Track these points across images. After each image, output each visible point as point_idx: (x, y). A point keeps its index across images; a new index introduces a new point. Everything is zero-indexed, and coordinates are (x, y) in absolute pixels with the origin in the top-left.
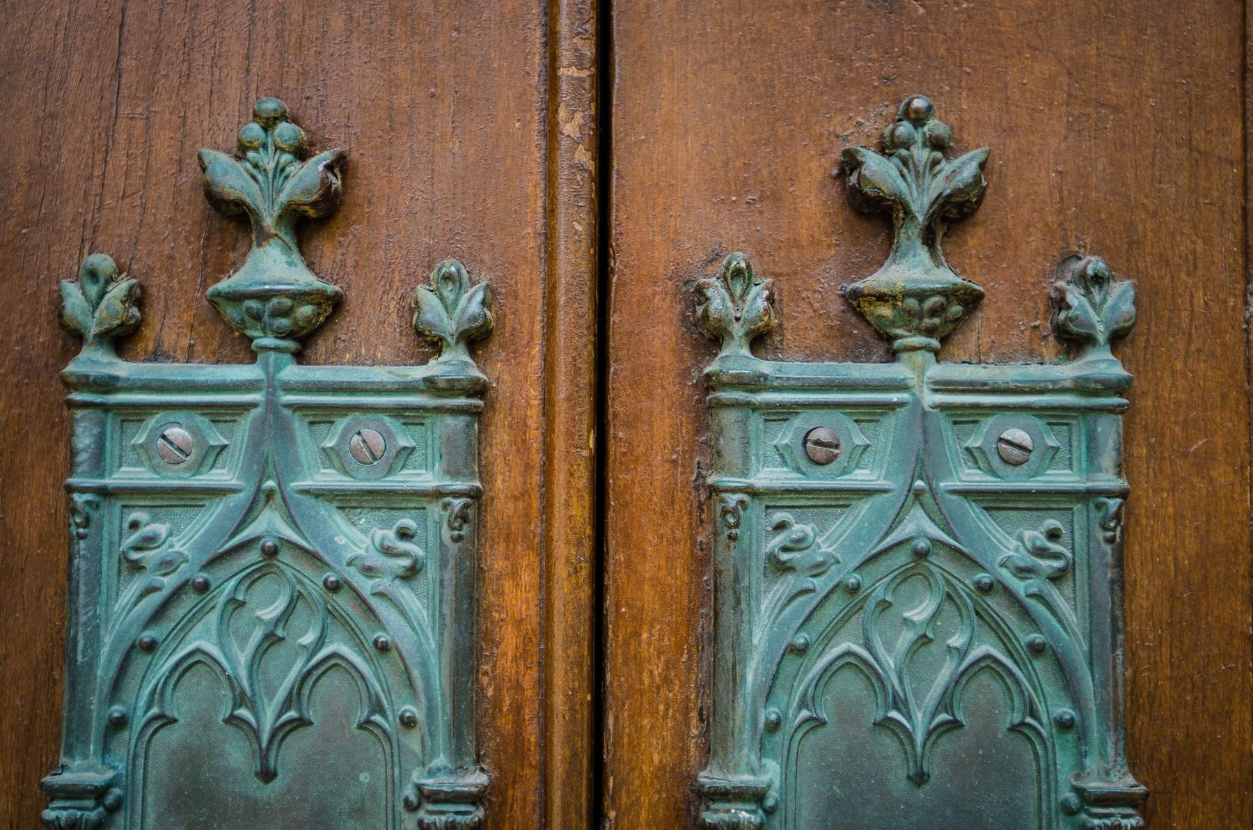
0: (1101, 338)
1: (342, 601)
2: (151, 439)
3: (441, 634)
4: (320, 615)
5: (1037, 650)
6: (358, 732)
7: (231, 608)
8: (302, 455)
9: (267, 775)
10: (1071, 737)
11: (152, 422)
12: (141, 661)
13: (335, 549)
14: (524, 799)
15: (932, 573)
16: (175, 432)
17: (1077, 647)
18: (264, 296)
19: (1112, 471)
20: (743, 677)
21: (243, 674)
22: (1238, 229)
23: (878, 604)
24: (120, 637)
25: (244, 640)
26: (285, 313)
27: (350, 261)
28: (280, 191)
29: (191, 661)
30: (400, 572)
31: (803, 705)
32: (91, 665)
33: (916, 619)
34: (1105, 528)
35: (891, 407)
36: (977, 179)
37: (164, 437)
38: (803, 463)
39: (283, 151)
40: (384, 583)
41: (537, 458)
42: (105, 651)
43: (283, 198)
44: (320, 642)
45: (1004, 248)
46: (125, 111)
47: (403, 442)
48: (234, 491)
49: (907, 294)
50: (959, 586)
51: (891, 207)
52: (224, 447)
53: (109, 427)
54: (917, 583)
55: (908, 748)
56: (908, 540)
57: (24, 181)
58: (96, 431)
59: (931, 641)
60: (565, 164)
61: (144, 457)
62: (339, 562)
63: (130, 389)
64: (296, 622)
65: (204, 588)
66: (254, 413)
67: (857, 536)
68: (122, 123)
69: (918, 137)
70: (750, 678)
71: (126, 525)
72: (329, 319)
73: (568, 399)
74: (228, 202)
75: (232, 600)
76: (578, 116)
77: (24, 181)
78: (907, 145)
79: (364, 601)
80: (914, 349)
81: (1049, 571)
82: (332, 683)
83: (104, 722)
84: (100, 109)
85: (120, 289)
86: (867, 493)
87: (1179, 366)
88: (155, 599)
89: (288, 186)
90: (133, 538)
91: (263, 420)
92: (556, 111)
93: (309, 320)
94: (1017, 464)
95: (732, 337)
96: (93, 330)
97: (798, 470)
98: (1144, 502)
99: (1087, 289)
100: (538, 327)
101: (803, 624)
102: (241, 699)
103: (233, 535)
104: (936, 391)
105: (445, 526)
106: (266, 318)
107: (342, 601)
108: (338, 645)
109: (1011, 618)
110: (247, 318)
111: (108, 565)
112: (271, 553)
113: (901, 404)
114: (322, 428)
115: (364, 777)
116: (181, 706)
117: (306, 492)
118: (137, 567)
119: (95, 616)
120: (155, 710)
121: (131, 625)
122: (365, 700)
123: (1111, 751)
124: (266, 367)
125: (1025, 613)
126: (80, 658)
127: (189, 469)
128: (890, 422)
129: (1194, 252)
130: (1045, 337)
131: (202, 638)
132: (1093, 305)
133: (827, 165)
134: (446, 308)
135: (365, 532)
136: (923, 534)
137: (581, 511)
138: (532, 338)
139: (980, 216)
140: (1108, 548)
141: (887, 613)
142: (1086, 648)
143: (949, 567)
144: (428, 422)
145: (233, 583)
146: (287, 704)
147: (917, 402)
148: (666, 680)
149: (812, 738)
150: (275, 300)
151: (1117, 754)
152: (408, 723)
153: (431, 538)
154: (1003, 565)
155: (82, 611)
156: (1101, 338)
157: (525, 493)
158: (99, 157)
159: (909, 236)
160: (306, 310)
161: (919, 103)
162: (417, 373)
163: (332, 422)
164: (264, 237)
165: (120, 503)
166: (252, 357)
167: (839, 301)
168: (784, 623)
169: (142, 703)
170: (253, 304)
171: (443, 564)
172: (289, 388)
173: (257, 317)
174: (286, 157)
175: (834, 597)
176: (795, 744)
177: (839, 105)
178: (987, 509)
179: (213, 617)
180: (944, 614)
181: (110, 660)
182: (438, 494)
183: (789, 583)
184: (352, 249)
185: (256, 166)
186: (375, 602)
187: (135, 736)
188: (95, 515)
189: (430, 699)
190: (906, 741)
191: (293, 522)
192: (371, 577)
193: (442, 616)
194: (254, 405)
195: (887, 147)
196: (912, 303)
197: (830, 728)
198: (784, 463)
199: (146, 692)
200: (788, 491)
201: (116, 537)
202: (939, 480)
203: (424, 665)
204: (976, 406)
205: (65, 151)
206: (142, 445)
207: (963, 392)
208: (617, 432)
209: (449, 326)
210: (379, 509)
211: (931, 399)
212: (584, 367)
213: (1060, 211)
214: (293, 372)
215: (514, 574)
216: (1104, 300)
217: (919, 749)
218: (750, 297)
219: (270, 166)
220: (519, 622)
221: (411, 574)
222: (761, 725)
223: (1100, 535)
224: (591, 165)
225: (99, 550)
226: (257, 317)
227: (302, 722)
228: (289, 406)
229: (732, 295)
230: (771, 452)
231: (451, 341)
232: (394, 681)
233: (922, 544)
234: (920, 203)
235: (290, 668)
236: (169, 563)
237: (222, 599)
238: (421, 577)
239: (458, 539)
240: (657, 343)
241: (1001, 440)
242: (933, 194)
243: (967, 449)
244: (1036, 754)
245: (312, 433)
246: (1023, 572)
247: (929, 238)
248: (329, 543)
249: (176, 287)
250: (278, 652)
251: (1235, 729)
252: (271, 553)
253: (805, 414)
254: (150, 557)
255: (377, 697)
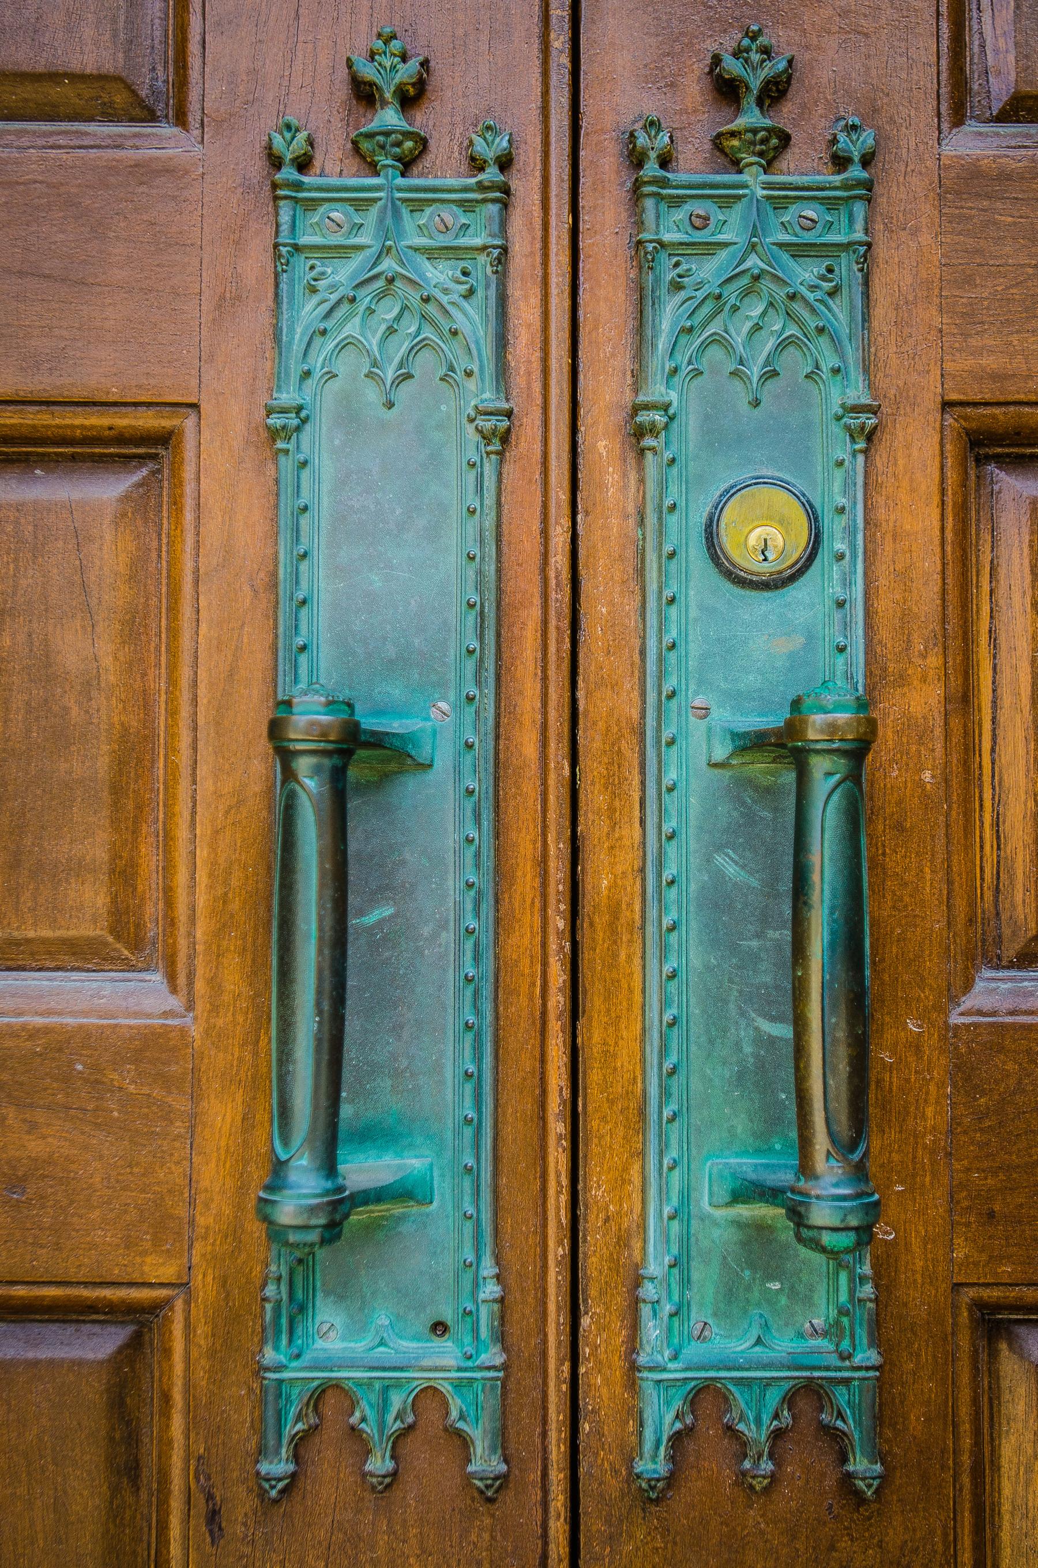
0: (856, 159)
1: (431, 309)
2: (321, 219)
3: (487, 326)
4: (418, 316)
5: (821, 330)
6: (439, 382)
7: (368, 313)
8: (407, 228)
9: (390, 405)
10: (839, 378)
11: (322, 210)
12: (318, 340)
13: (426, 279)
14: (533, 423)
15: (761, 290)
16: (334, 215)
17: (844, 331)
18: (387, 134)
19: (862, 232)
20: (657, 345)
21: (375, 348)
22: (935, 103)
23: (732, 307)
24: (306, 328)
25: (376, 331)
26: (398, 144)
27: (431, 123)
28: (393, 79)
29: (346, 342)
30: (463, 293)
31: (690, 363)
32: (290, 343)
33: (753, 314)
34: (858, 263)
35: (739, 197)
36: (786, 70)
37: (329, 218)
38: (690, 229)
39: (395, 55)
40: (455, 297)
41: (539, 234)
42: (297, 337)
43: (397, 81)
44: (418, 332)
45: (803, 113)
46: (301, 38)
47: (464, 221)
48: (369, 247)
49: (747, 131)
50: (777, 297)
51: (738, 87)
52: (362, 225)
53: (298, 212)
54: (753, 297)
55: (749, 385)
56: (748, 270)
57: (245, 78)
58: (291, 213)
59: (761, 328)
60: (555, 65)
61: (317, 229)
62: (429, 285)
63: (309, 190)
64: (404, 322)
65: (353, 300)
66: (380, 203)
67: (720, 268)
68: (300, 46)
69: (754, 47)
70: (660, 346)
71: (307, 269)
72: (421, 153)
73: (557, 196)
74: (365, 83)
75: (368, 308)
76: (562, 37)
77: (245, 78)
78: (748, 50)
79: (442, 307)
80: (751, 164)
81: (827, 289)
82: (425, 355)
83: (299, 372)
84: (288, 38)
85: (302, 136)
86: (726, 245)
87: (901, 179)
88: (326, 306)
89: (399, 75)
90: (313, 274)
91: (385, 207)
92: (549, 35)
93: (411, 151)
94: (809, 230)
95: (649, 159)
96: (289, 156)
97: (687, 233)
98: (882, 255)
99: (848, 132)
100: (538, 159)
101: (690, 315)
102: (375, 364)
103: (369, 271)
104: (764, 188)
105: (488, 265)
106: (388, 147)
107: (431, 309)
108: (428, 332)
109: (806, 314)
110: (377, 148)
111: (299, 289)
112: (391, 281)
113: (744, 196)
114: (417, 214)
115: (444, 408)
116: (341, 367)
117: (410, 247)
118: (314, 290)
119: (292, 316)
120: (326, 370)
121: (312, 320)
122: (444, 363)
123: (861, 385)
124: (387, 178)
125: (813, 311)
126: (284, 338)
127: (343, 235)
128: (739, 207)
129: (909, 116)
130: (826, 163)
131: (352, 328)
132: (852, 141)
133: (700, 67)
134: (488, 144)
135: (441, 272)
136: (755, 266)
137: (565, 259)
138: (535, 166)
139: (789, 95)
140: (859, 275)
141: (737, 313)
142: (848, 331)
143: (771, 286)
144: (477, 210)
145: (369, 298)
146: (401, 366)
147: (753, 194)
148: (613, 355)
149: (695, 382)
150: (393, 136)
151: (864, 387)
152: (469, 374)
153: (480, 275)
154: (801, 284)
155: (285, 312)
156: (856, 159)
157: (532, 253)
158: (288, 64)
159: (749, 101)
160: (409, 144)
161: (755, 28)
162: (473, 180)
163: (423, 210)
164: (384, 103)
165: (304, 256)
166: (377, 174)
167: (710, 143)
168: (679, 315)
169: (319, 365)
170: (381, 138)
171: (487, 287)
172: (400, 189)
173: (382, 147)
174: (397, 59)
175: (707, 302)
176: (686, 384)
177: (710, 33)
178: (793, 256)
179: (357, 320)
180: (769, 314)
181: (301, 340)
182: (484, 248)
183: (683, 295)
184: (432, 116)
185: (380, 64)
186: (449, 307)
187: (315, 383)
188: (291, 260)
189: (481, 361)
190: (747, 382)
191: (402, 264)
192: (447, 294)
193: (487, 315)
194: (380, 199)
195: (736, 54)
196: (749, 135)
197: (705, 375)
198: (679, 230)
199: (321, 359)
200: (681, 244)
201: (302, 274)
202: (765, 237)
203: (477, 343)
204: (786, 197)
205: (267, 61)
206: (316, 223)
207: (780, 189)
208: (584, 216)
209: (490, 154)
210: (450, 259)
211: (761, 193)
212: (566, 178)
213: (835, 93)
214: (400, 181)
215: (526, 297)
216: (858, 139)
217: (755, 385)
218: (659, 137)
219: (388, 65)
220: (529, 326)
221: (471, 292)
222: (667, 370)
223: (855, 267)
224: (569, 65)
225: (293, 280)
226: (382, 147)
227: (409, 376)
228: (399, 199)
229: (649, 136)
230: (671, 224)
231: (492, 163)
232: (461, 353)
233: (756, 271)
234: (756, 84)
235: (401, 347)
236: (334, 286)
237: (362, 308)
238: (474, 297)
239: (497, 272)
240: (607, 167)
241: (800, 216)
242: (762, 79)
243: (782, 223)
244: (820, 390)
245: (412, 217)
246: (813, 288)
247: (760, 102)
248: (422, 276)
249: (332, 137)
250: (394, 338)
251: (931, 380)
252: (391, 281)
253: (691, 201)
254: (321, 284)
255: (451, 362)
